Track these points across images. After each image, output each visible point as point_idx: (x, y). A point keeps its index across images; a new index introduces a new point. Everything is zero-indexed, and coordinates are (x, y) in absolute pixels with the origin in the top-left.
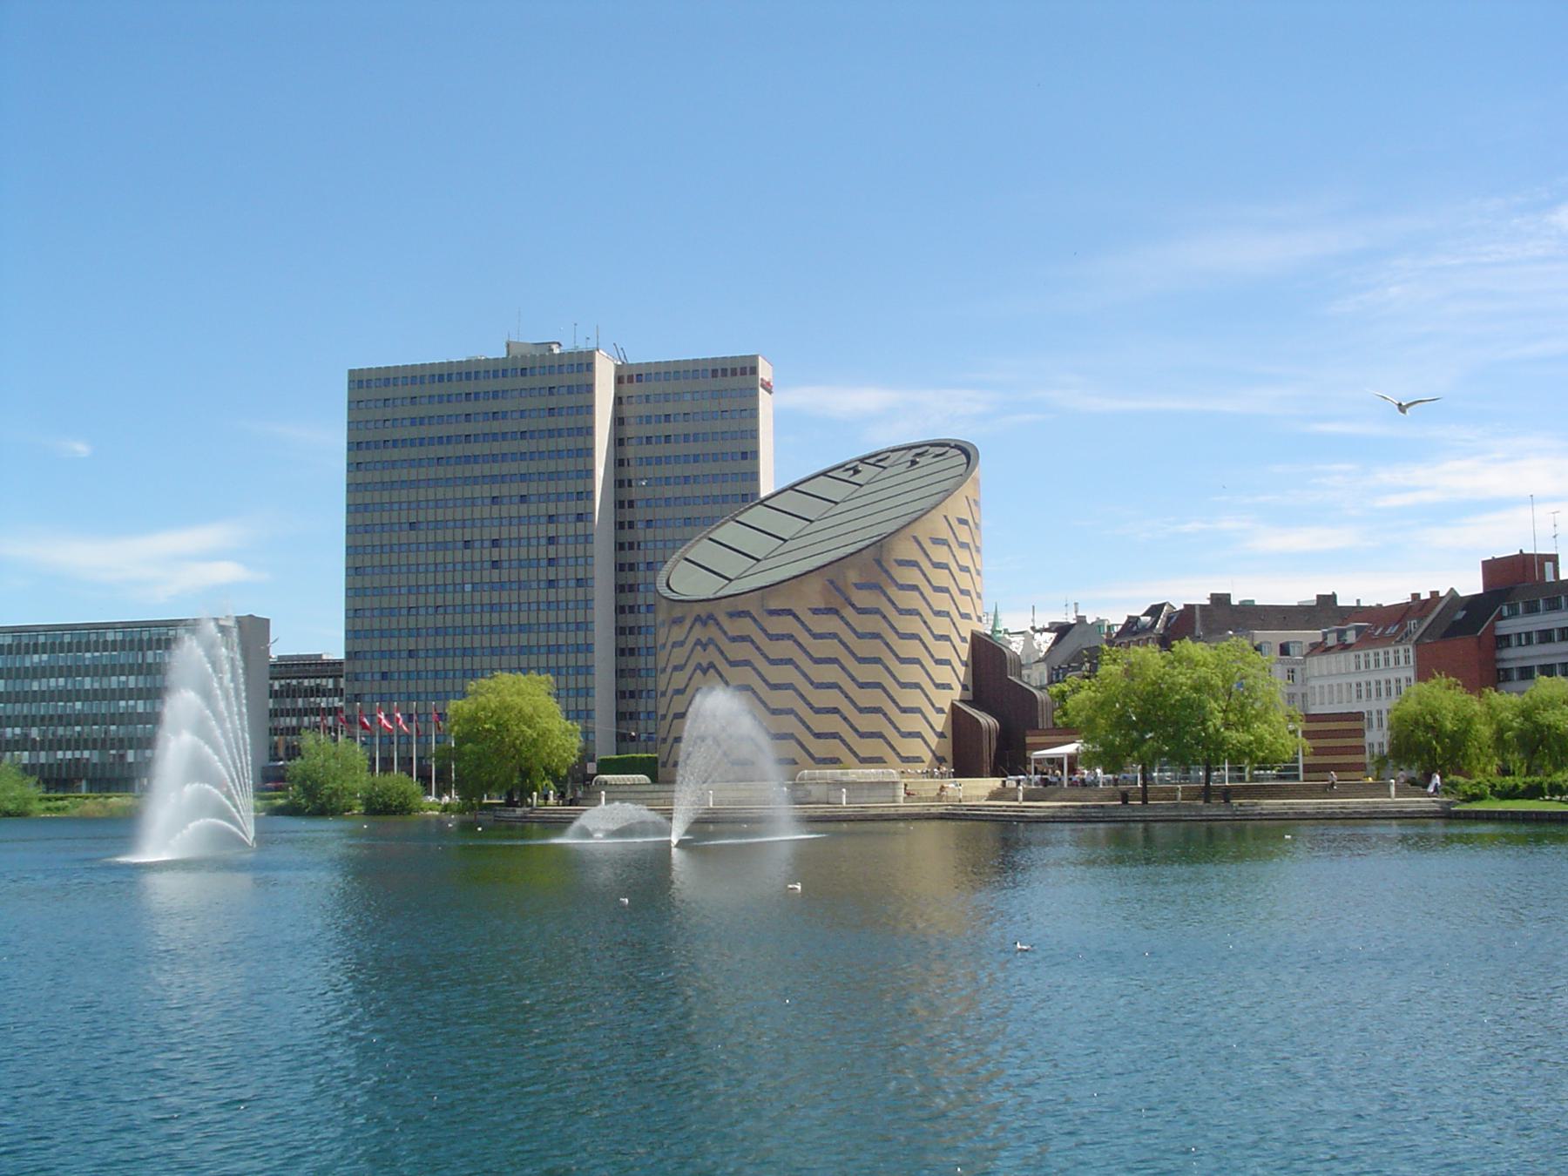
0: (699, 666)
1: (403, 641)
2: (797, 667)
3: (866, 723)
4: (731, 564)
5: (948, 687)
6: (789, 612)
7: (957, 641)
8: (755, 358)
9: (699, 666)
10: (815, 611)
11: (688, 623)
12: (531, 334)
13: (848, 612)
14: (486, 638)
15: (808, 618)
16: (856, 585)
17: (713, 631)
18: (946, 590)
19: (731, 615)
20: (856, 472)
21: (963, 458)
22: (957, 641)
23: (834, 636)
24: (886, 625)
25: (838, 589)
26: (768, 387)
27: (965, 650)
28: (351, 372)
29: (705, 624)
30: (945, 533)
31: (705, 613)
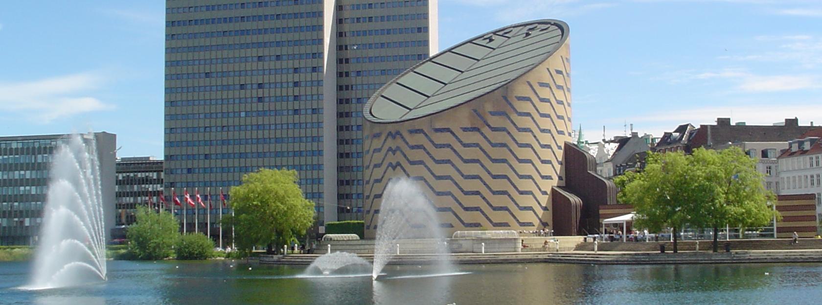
2: (453, 165)
4: (412, 99)
5: (550, 178)
9: (390, 165)
10: (465, 129)
11: (383, 137)
13: (486, 130)
16: (490, 113)
17: (399, 142)
18: (548, 116)
19: (411, 132)
20: (491, 40)
21: (559, 32)
25: (479, 115)
27: (560, 154)
30: (547, 79)
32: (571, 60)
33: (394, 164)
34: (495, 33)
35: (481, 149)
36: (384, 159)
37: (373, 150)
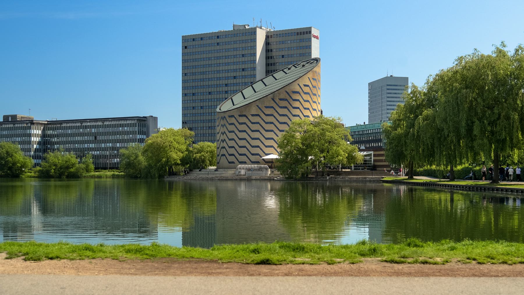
1: (199, 124)
2: (247, 133)
6: (245, 116)
8: (310, 28)
10: (253, 115)
12: (240, 22)
14: (207, 124)
15: (250, 117)
18: (308, 109)
19: (229, 117)
23: (258, 123)
24: (275, 120)
26: (317, 37)
35: (260, 125)
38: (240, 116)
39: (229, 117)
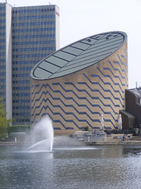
0: (44, 99)
2: (74, 100)
3: (94, 109)
4: (54, 69)
5: (118, 106)
6: (72, 84)
7: (121, 93)
9: (44, 99)
10: (79, 83)
11: (40, 87)
15: (77, 85)
17: (48, 89)
19: (53, 84)
20: (89, 41)
21: (122, 37)
22: (121, 93)
27: (123, 95)
28: (118, 38)
29: (46, 87)
30: (117, 59)
31: (45, 84)
32: (129, 86)
33: (45, 99)
34: (91, 37)
36: (41, 97)
37: (36, 98)
38: (66, 83)
39: (53, 84)
